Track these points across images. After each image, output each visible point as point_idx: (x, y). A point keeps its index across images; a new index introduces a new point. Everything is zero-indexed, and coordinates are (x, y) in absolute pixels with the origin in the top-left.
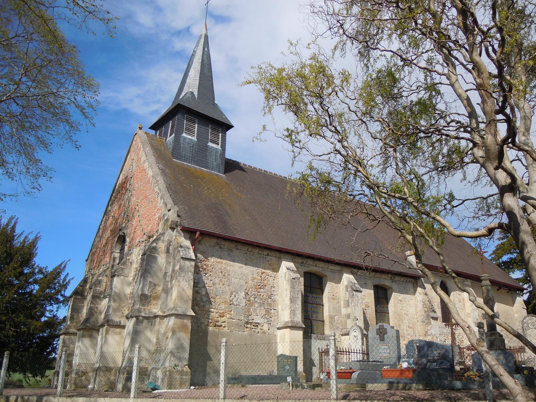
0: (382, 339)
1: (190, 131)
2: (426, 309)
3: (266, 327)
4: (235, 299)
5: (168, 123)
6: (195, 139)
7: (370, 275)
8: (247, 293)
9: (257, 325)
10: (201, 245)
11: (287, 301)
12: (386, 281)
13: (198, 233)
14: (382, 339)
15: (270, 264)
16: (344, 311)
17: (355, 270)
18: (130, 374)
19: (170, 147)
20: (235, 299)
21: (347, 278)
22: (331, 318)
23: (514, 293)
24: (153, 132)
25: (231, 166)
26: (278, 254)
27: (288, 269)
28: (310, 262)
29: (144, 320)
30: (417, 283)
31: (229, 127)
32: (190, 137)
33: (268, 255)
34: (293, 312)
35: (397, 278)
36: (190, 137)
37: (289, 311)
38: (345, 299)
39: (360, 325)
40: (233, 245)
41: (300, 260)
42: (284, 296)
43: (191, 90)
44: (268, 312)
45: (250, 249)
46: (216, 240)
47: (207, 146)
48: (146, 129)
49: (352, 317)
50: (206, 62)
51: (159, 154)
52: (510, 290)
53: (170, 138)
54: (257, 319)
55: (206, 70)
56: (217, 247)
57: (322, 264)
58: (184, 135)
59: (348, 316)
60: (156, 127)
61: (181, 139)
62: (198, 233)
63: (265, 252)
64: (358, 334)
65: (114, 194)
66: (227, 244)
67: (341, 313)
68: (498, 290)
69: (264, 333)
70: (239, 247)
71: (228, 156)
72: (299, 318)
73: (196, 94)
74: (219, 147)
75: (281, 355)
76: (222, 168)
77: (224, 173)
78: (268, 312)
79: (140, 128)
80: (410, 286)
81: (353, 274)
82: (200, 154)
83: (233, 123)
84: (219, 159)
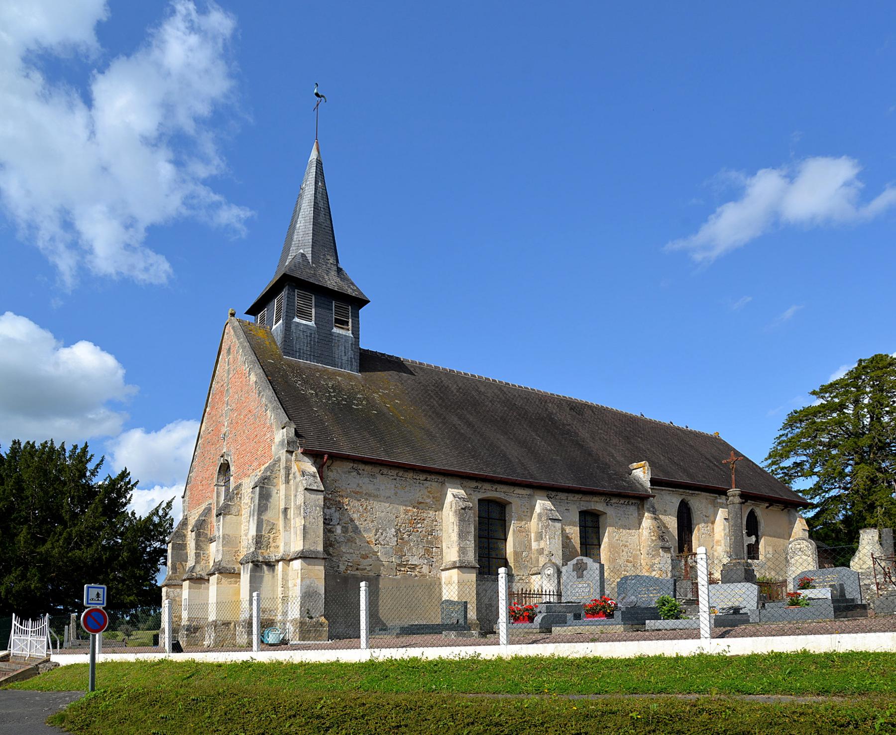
0: (580, 576)
1: (305, 315)
2: (654, 538)
3: (425, 569)
4: (383, 537)
5: (271, 304)
6: (312, 324)
7: (575, 499)
8: (399, 529)
9: (413, 567)
10: (332, 471)
11: (454, 537)
12: (597, 505)
13: (326, 457)
14: (580, 576)
15: (429, 492)
16: (534, 545)
17: (554, 494)
18: (250, 624)
19: (279, 339)
20: (383, 537)
21: (542, 505)
22: (516, 554)
23: (793, 511)
24: (251, 318)
25: (370, 361)
26: (441, 479)
27: (454, 496)
28: (487, 486)
29: (261, 565)
30: (643, 507)
31: (360, 302)
32: (304, 322)
33: (426, 480)
34: (462, 551)
35: (614, 500)
36: (304, 322)
37: (457, 549)
38: (537, 530)
39: (557, 562)
40: (376, 470)
41: (474, 484)
42: (451, 531)
43: (302, 251)
44: (428, 551)
45: (400, 474)
46: (352, 465)
47: (331, 334)
48: (241, 315)
49: (546, 552)
50: (321, 205)
51: (259, 353)
52: (786, 507)
53: (277, 327)
54: (414, 561)
55: (321, 219)
56: (355, 473)
57: (505, 488)
58: (297, 320)
59: (541, 551)
60: (254, 310)
61: (293, 328)
62: (326, 457)
63: (422, 477)
64: (550, 571)
65: (208, 409)
66: (368, 468)
67: (530, 548)
68: (767, 507)
69: (424, 576)
70: (385, 471)
71: (363, 345)
72: (471, 557)
73: (309, 257)
74: (349, 333)
75: (447, 601)
76: (356, 364)
77: (360, 371)
78: (428, 551)
79: (233, 315)
80: (632, 510)
81: (464, 488)
82: (323, 346)
83: (368, 295)
84: (350, 354)
